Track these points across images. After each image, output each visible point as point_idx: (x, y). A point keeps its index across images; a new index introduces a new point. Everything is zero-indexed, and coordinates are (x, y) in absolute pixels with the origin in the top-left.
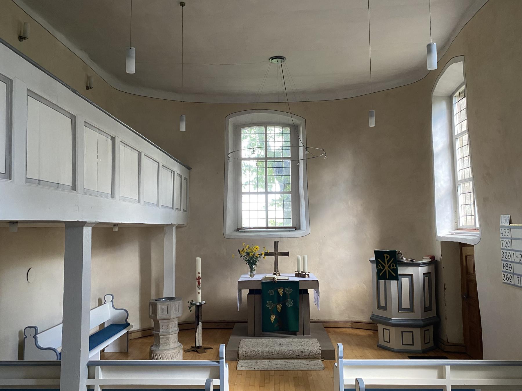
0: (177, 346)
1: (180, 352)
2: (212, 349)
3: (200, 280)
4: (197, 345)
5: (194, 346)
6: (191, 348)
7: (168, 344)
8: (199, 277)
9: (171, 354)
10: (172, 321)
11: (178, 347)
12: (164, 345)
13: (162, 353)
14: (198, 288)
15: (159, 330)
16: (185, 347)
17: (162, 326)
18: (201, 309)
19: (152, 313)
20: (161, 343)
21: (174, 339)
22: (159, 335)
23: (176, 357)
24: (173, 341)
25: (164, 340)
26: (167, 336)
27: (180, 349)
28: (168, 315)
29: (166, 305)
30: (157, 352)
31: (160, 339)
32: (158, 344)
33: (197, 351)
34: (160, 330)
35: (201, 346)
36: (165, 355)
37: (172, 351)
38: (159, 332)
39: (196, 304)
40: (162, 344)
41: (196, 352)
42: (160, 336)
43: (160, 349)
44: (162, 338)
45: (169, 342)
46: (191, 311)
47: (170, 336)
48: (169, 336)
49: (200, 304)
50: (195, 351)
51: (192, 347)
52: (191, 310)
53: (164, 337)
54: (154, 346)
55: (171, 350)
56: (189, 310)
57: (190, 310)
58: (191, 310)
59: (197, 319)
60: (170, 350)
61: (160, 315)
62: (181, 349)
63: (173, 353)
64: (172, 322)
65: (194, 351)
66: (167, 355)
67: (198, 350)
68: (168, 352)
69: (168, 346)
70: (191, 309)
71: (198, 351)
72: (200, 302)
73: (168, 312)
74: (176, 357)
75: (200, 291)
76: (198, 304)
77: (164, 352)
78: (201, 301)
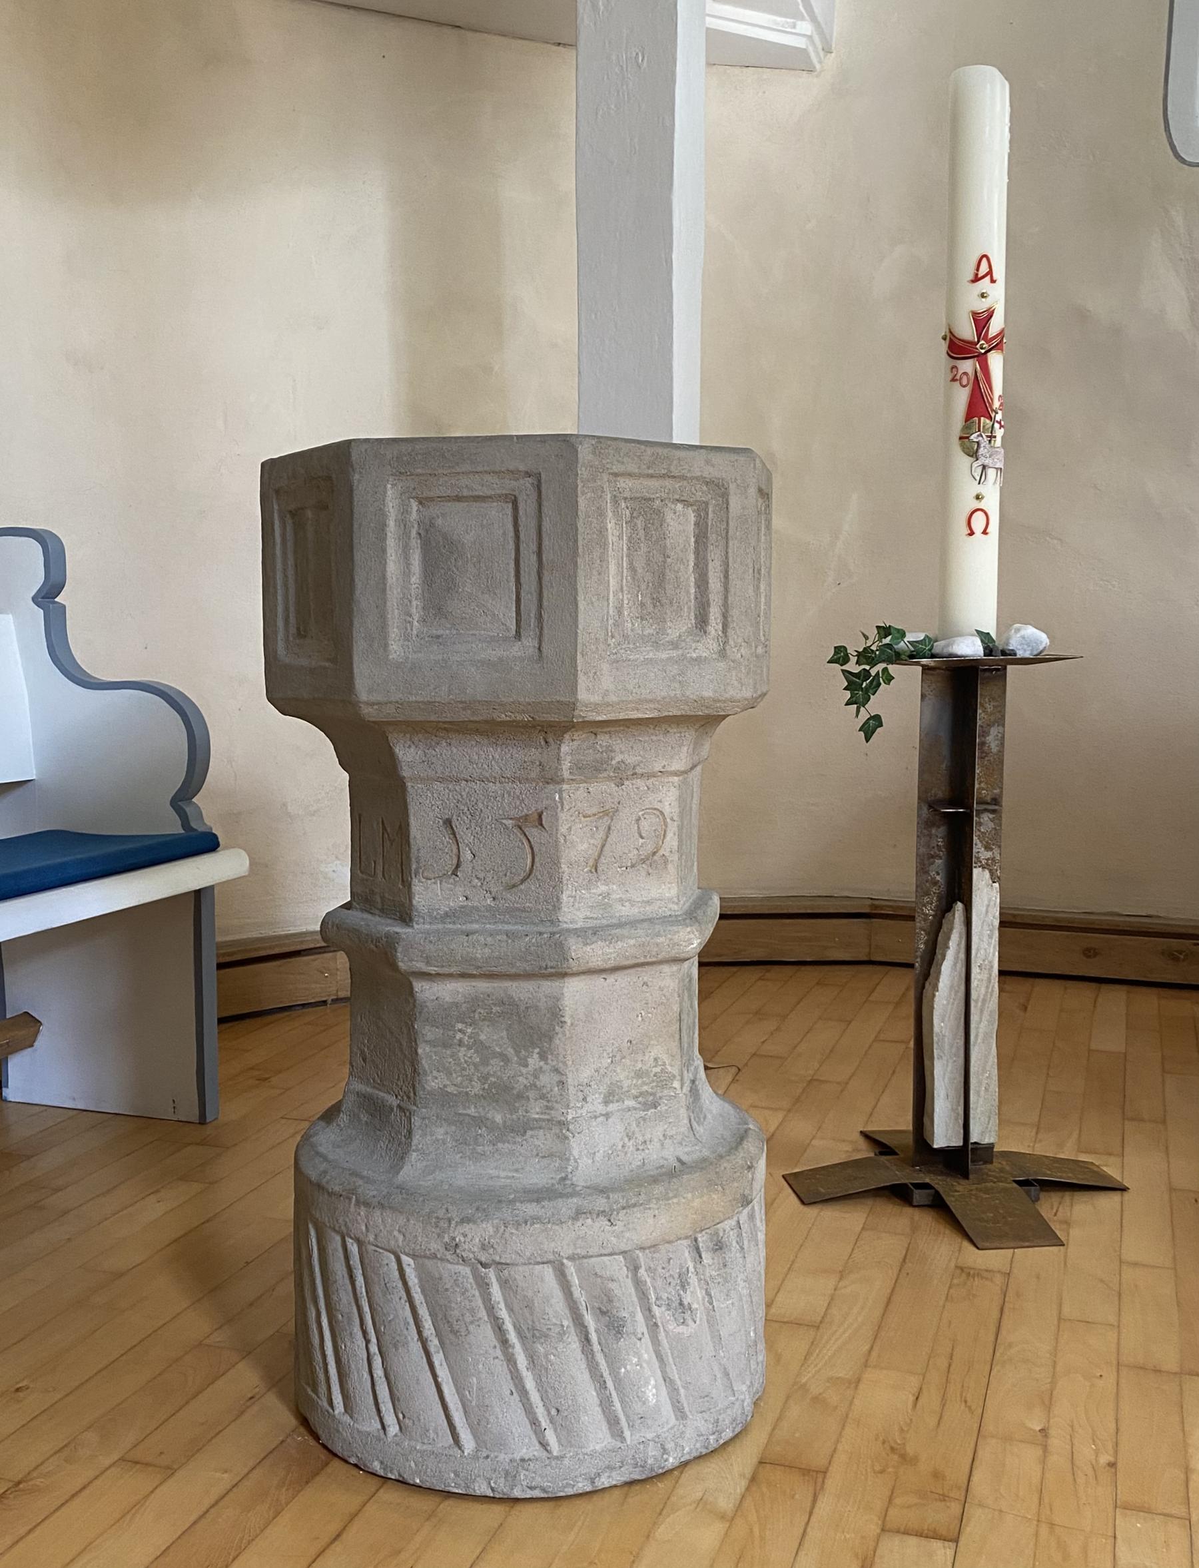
0: (689, 1152)
1: (719, 1246)
2: (1123, 1189)
3: (996, 361)
4: (944, 1135)
5: (906, 1123)
6: (865, 1151)
7: (535, 1110)
8: (982, 321)
9: (571, 1268)
10: (590, 771)
11: (702, 1165)
12: (480, 1121)
13: (435, 1246)
14: (967, 460)
15: (408, 885)
16: (800, 1128)
17: (448, 823)
18: (1001, 721)
19: (301, 634)
20: (433, 1081)
21: (635, 1047)
22: (393, 966)
23: (653, 1327)
24: (622, 1075)
25: (479, 1046)
26: (521, 990)
27: (717, 1201)
28: (529, 642)
29: (496, 486)
30: (359, 1220)
31: (428, 1032)
32: (392, 1101)
33: (938, 1205)
34: (418, 887)
35: (990, 1147)
36: (483, 1285)
37: (594, 1228)
38: (405, 916)
39: (938, 647)
40: (445, 1099)
41: (926, 1220)
42: (418, 986)
43: (412, 1170)
44: (449, 1015)
45: (546, 1080)
46: (871, 727)
47: (574, 992)
48: (547, 986)
49: (989, 651)
50: (918, 1195)
51: (880, 1145)
52: (877, 721)
53: (475, 1002)
54: (343, 1118)
55: (579, 1214)
56: (851, 719)
57: (864, 715)
58: (877, 721)
59: (939, 835)
60: (566, 1207)
61: (396, 649)
62: (746, 1201)
63: (617, 1267)
64: (603, 788)
65: (900, 1194)
66: (504, 1284)
67: (956, 1191)
68: (523, 1243)
69: (542, 1140)
70: (875, 705)
71: (950, 1201)
72: (985, 637)
73: (529, 600)
74: (653, 1327)
75: (992, 503)
76: (970, 648)
77: (473, 1236)
78: (1006, 619)
